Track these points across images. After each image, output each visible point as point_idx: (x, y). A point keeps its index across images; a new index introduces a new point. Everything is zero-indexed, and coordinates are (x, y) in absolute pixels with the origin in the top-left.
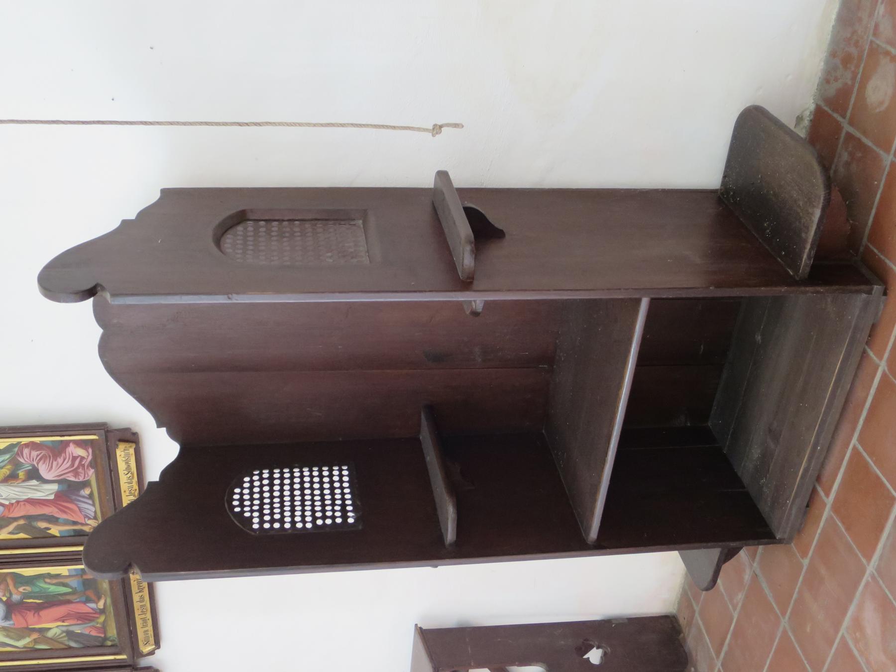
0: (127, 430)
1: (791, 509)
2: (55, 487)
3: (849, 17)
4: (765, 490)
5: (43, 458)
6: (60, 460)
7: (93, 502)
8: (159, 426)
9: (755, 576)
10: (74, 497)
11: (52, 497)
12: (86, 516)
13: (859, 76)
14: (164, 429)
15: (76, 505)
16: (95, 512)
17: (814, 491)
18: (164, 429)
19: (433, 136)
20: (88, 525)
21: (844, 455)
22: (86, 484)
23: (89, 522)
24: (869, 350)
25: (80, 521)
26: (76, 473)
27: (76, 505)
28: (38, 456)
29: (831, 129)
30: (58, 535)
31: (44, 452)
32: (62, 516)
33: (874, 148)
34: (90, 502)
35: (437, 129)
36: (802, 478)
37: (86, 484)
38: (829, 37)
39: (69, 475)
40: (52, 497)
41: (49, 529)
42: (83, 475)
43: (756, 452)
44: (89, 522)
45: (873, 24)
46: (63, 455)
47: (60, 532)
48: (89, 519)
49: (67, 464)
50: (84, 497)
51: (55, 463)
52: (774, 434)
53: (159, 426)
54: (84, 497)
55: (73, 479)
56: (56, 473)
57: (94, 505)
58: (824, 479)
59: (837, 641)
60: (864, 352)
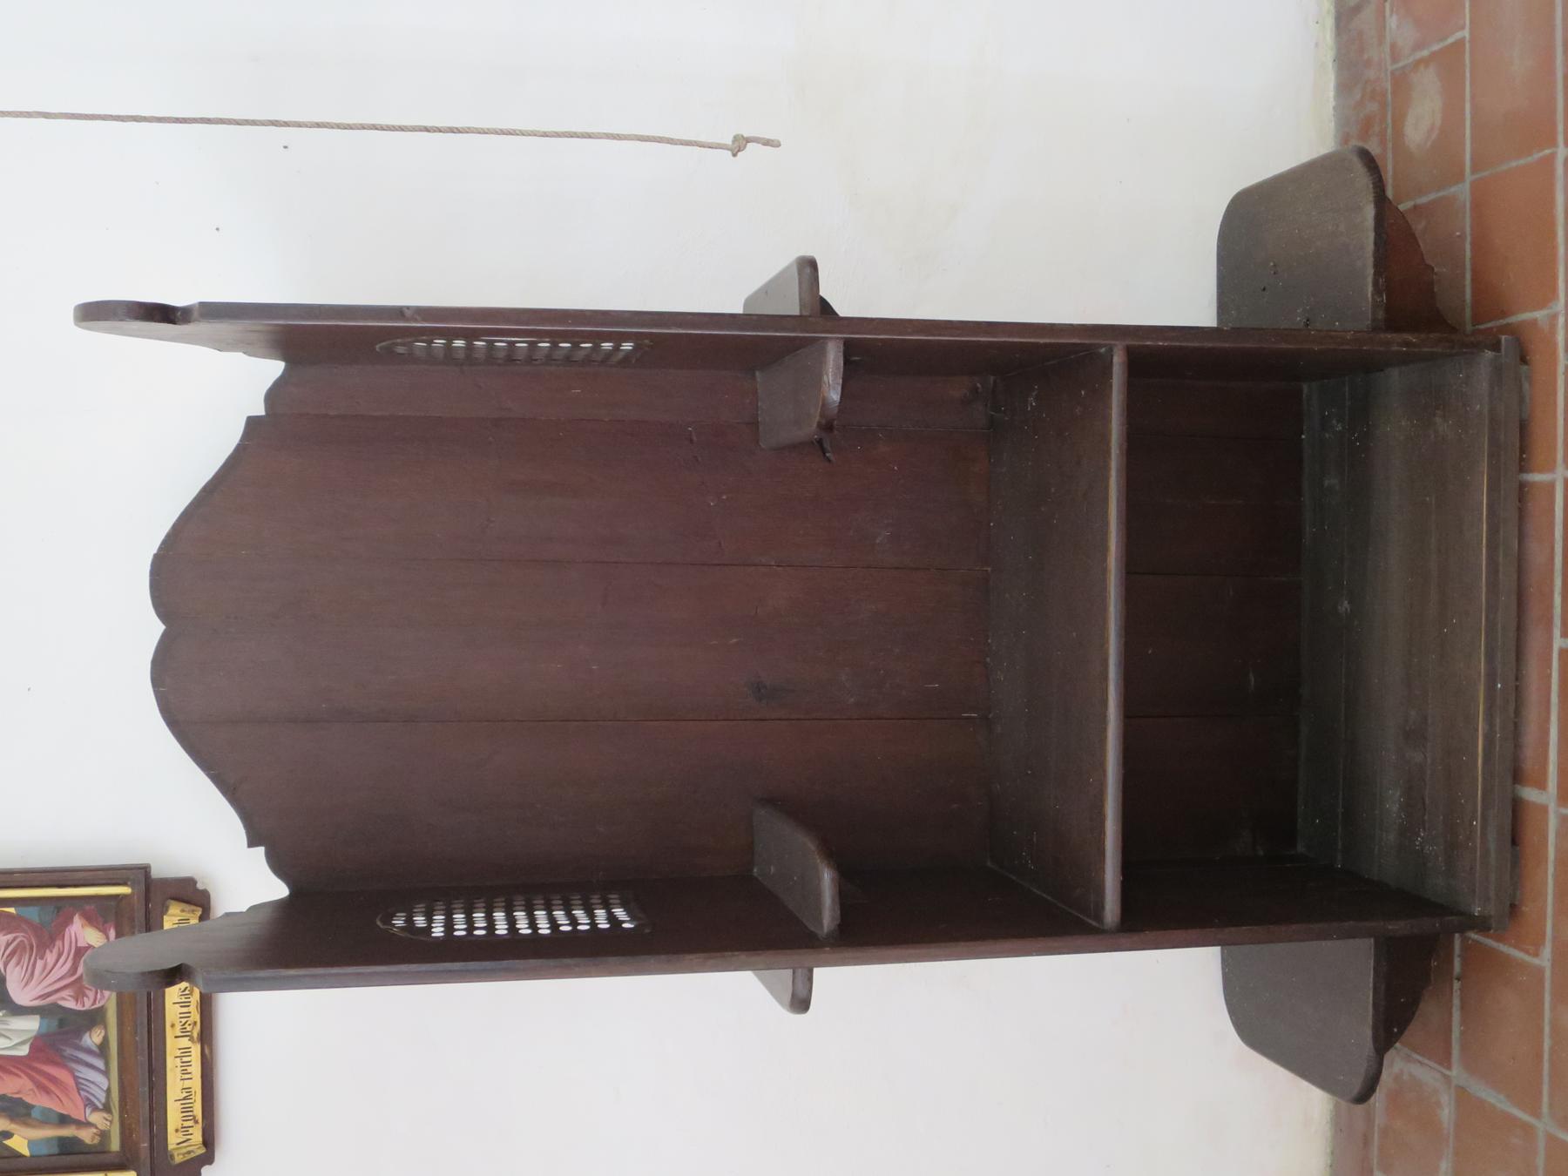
0: (190, 882)
1: (1484, 834)
2: (31, 1025)
3: (1345, 16)
4: (1428, 849)
5: (14, 953)
6: (50, 957)
7: (107, 1064)
8: (252, 843)
9: (1463, 1098)
10: (69, 1051)
11: (24, 1051)
12: (89, 1103)
13: (1389, 131)
14: (261, 850)
15: (72, 1072)
16: (108, 1091)
17: (1517, 808)
18: (260, 851)
19: (734, 155)
20: (89, 1124)
21: (1549, 687)
22: (94, 1018)
23: (95, 1118)
24: (1513, 319)
25: (75, 1115)
26: (79, 995)
27: (72, 1072)
28: (8, 945)
29: (1365, 161)
30: (26, 1152)
31: (21, 936)
32: (40, 1101)
33: (1440, 194)
34: (100, 1064)
35: (739, 145)
36: (1485, 762)
37: (94, 1018)
38: (1332, 125)
39: (65, 994)
40: (24, 1051)
41: (8, 1135)
42: (91, 994)
43: (1393, 802)
44: (95, 1118)
45: (1387, 49)
46: (58, 943)
47: (31, 1144)
48: (95, 1109)
49: (63, 968)
50: (89, 1051)
51: (40, 963)
52: (1414, 735)
53: (252, 843)
54: (89, 1051)
55: (70, 1004)
56: (39, 990)
57: (106, 1073)
58: (1529, 765)
59: (1537, 156)
60: (1522, 486)
